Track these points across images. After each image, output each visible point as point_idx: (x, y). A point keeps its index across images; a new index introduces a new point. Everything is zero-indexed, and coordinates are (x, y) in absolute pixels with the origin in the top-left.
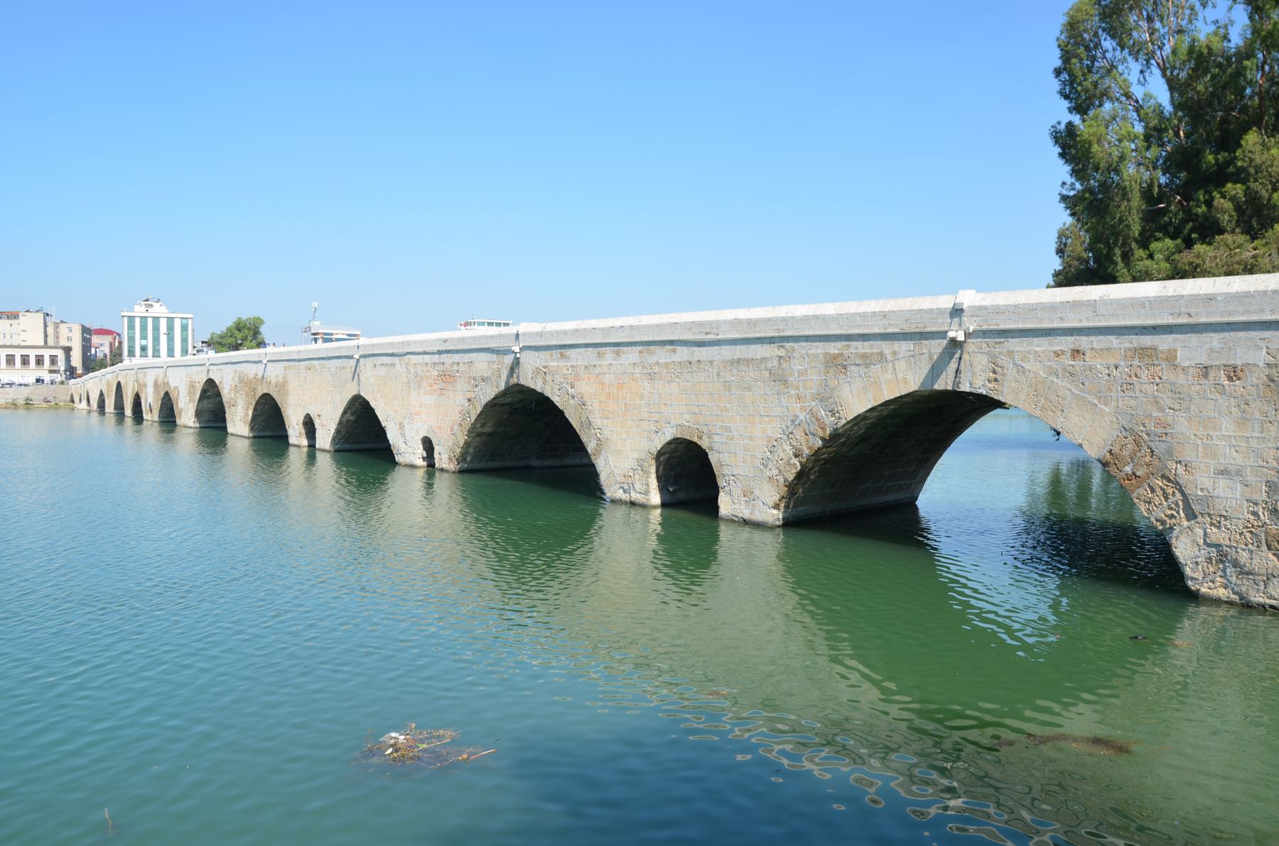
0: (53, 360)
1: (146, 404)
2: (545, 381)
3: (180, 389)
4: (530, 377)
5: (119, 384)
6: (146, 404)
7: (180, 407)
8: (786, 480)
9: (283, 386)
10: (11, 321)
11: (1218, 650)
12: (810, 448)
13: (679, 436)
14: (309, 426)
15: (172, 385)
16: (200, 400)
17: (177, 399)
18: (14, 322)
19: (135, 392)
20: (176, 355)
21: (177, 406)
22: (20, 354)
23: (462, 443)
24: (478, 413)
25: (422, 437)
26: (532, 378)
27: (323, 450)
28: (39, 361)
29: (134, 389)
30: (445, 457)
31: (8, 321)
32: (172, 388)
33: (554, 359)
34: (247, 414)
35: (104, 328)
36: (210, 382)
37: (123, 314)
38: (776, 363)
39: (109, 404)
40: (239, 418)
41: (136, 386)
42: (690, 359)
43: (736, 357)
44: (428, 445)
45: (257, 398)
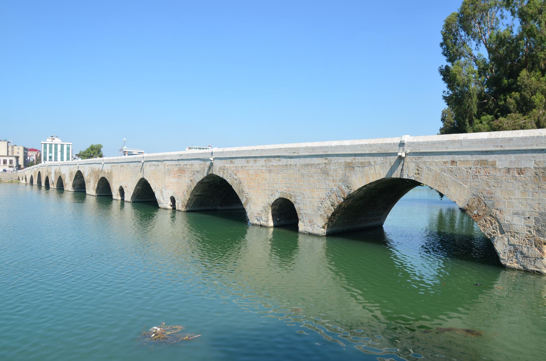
0: (11, 162)
2: (224, 173)
6: (51, 181)
8: (328, 216)
13: (282, 197)
15: (63, 173)
16: (74, 179)
17: (65, 179)
24: (195, 186)
29: (46, 175)
30: (180, 205)
34: (95, 186)
35: (33, 148)
37: (42, 142)
38: (324, 166)
39: (35, 181)
40: (91, 187)
43: (306, 163)
44: (173, 200)
45: (99, 179)
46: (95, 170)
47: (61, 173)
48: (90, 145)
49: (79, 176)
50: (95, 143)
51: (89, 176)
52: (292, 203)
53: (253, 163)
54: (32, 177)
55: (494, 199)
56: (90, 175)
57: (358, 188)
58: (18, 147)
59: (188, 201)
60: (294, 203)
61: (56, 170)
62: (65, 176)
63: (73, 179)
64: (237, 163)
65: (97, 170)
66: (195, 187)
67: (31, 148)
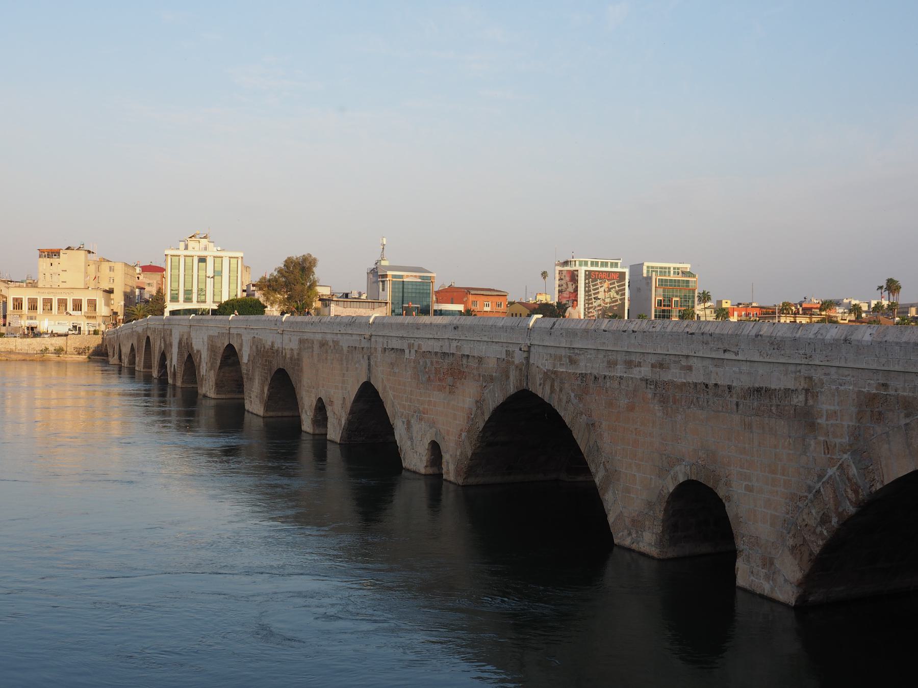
0: (92, 303)
1: (171, 366)
2: (552, 390)
3: (202, 353)
4: (538, 384)
5: (148, 338)
6: (171, 366)
7: (202, 373)
8: (811, 554)
9: (297, 362)
10: (52, 260)
11: (840, 304)
12: (839, 515)
13: (694, 478)
14: (321, 408)
15: (195, 348)
16: (220, 368)
17: (199, 366)
18: (55, 260)
19: (162, 352)
20: (207, 300)
21: (199, 372)
22: (57, 298)
23: (469, 454)
24: (486, 419)
25: (429, 441)
26: (540, 385)
27: (332, 442)
28: (78, 306)
29: (160, 348)
30: (452, 467)
31: (48, 259)
32: (195, 352)
33: (563, 364)
34: (263, 391)
35: (154, 264)
36: (230, 347)
37: (167, 252)
38: (802, 398)
39: (140, 361)
40: (255, 394)
41: (163, 345)
42: (706, 382)
43: (757, 385)
44: (435, 448)
45: (273, 373)
46: (264, 347)
47: (192, 348)
48: (305, 253)
49: (230, 355)
50: (297, 253)
51: (251, 362)
52: (721, 500)
53: (624, 370)
54: (132, 349)
55: (729, 345)
56: (252, 360)
57: (892, 479)
58: (111, 264)
59: (471, 460)
60: (724, 501)
61: (183, 335)
62: (200, 356)
63: (218, 367)
64: (586, 366)
65: (267, 347)
66: (487, 422)
67: (148, 264)
